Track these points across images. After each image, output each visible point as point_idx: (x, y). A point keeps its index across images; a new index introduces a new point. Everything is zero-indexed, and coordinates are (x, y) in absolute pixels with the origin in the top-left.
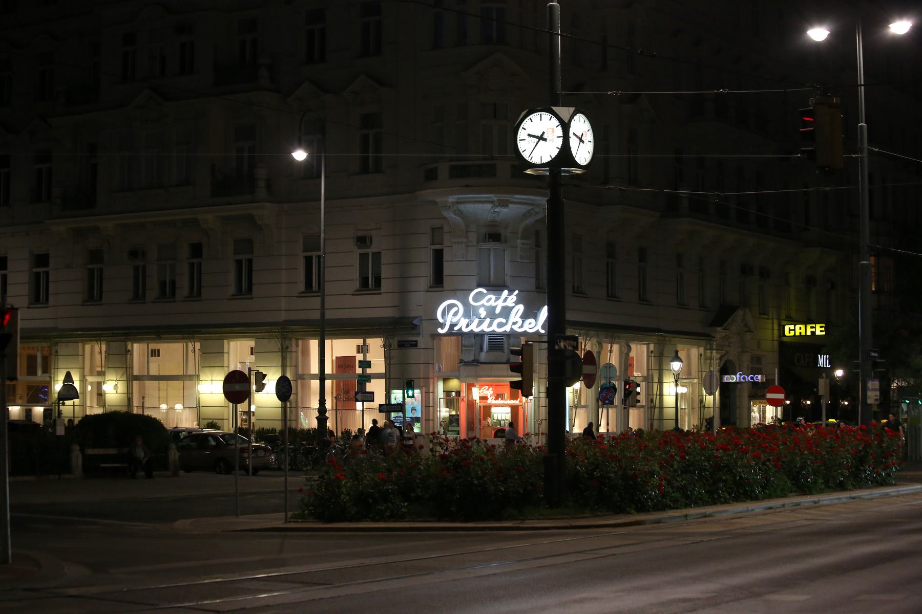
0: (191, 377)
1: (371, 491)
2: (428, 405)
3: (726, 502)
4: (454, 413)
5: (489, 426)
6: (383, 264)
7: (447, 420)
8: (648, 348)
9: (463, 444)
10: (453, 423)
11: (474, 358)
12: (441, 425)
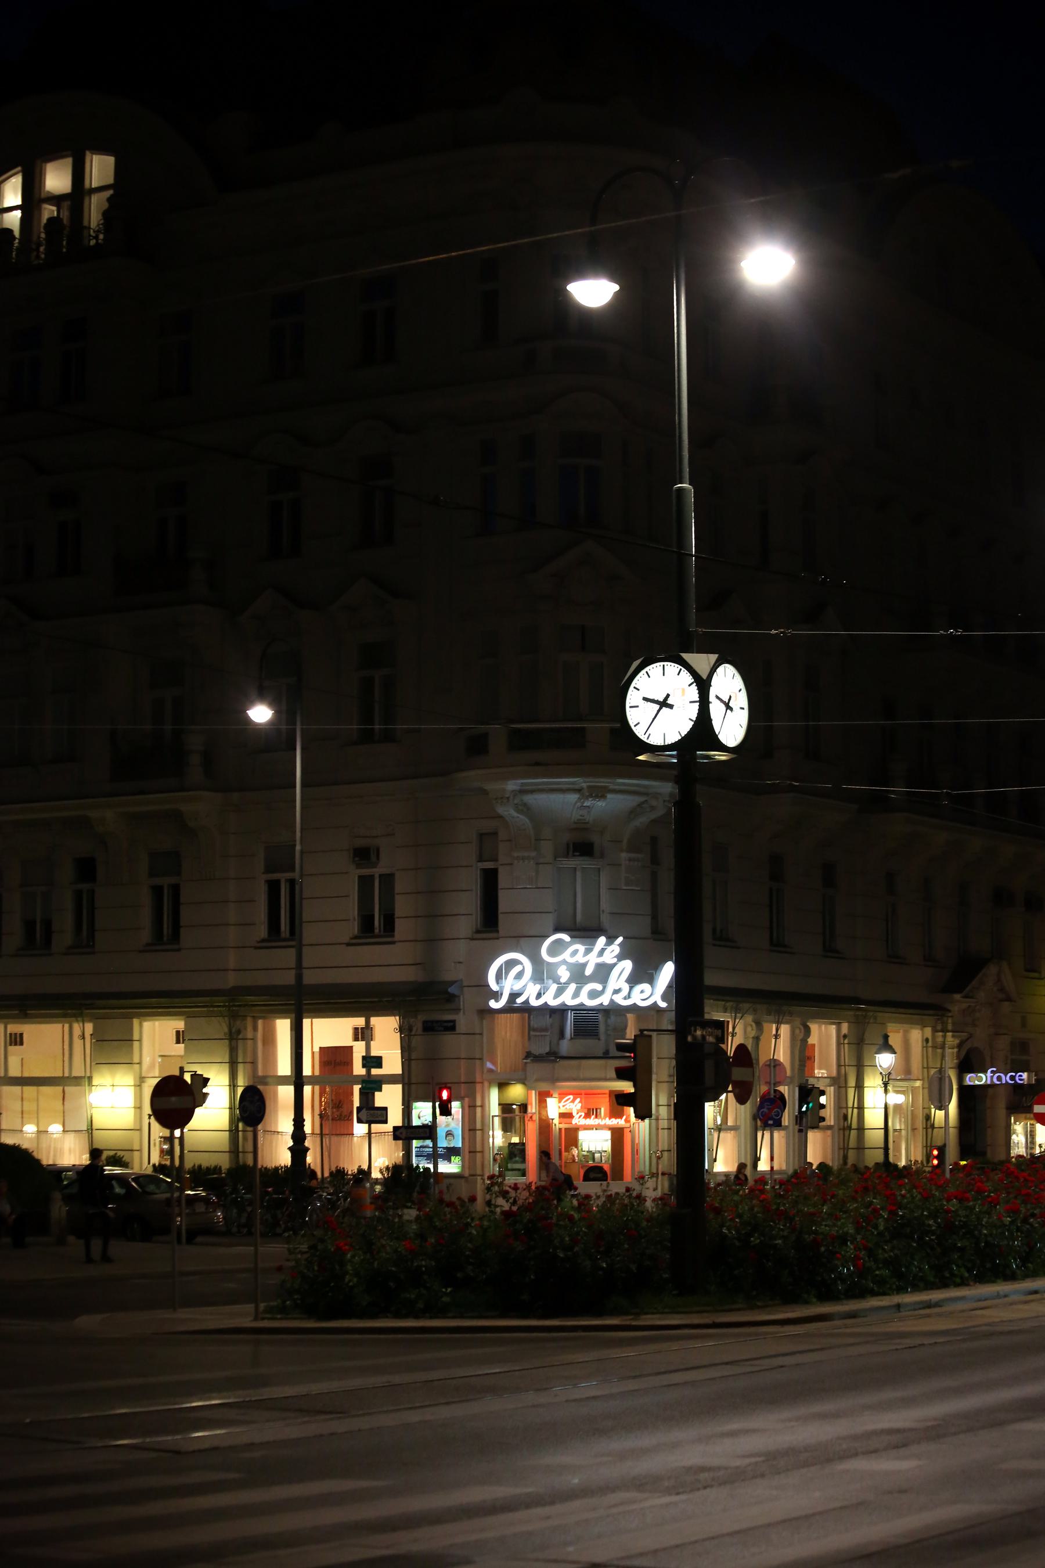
0: (77, 1081)
1: (393, 1269)
2: (473, 1128)
3: (963, 1283)
4: (515, 1140)
5: (574, 1161)
7: (506, 1151)
8: (838, 1031)
10: (515, 1156)
11: (550, 1050)
12: (495, 1160)
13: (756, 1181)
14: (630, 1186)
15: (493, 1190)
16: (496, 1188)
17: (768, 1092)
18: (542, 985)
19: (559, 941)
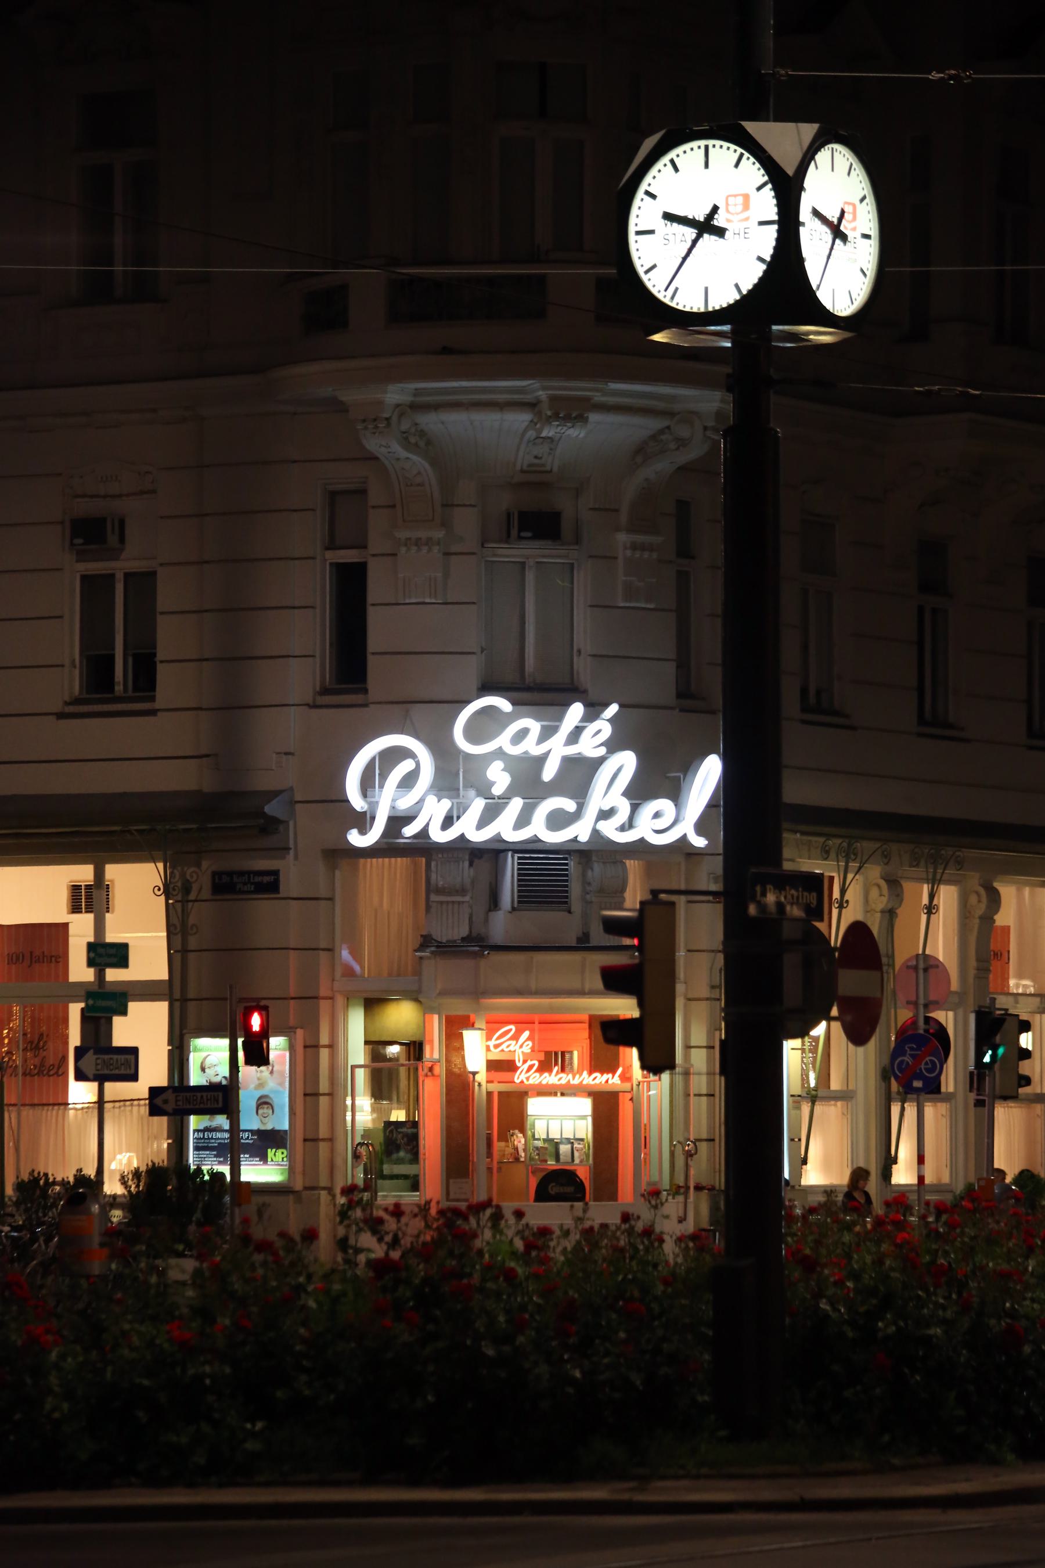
1: (146, 1382)
4: (399, 1115)
5: (517, 1159)
6: (162, 613)
7: (380, 1138)
9: (449, 1224)
10: (398, 1148)
12: (356, 1156)
13: (887, 1204)
14: (631, 1210)
15: (353, 1218)
16: (358, 1213)
17: (914, 1022)
18: (455, 801)
19: (488, 711)
